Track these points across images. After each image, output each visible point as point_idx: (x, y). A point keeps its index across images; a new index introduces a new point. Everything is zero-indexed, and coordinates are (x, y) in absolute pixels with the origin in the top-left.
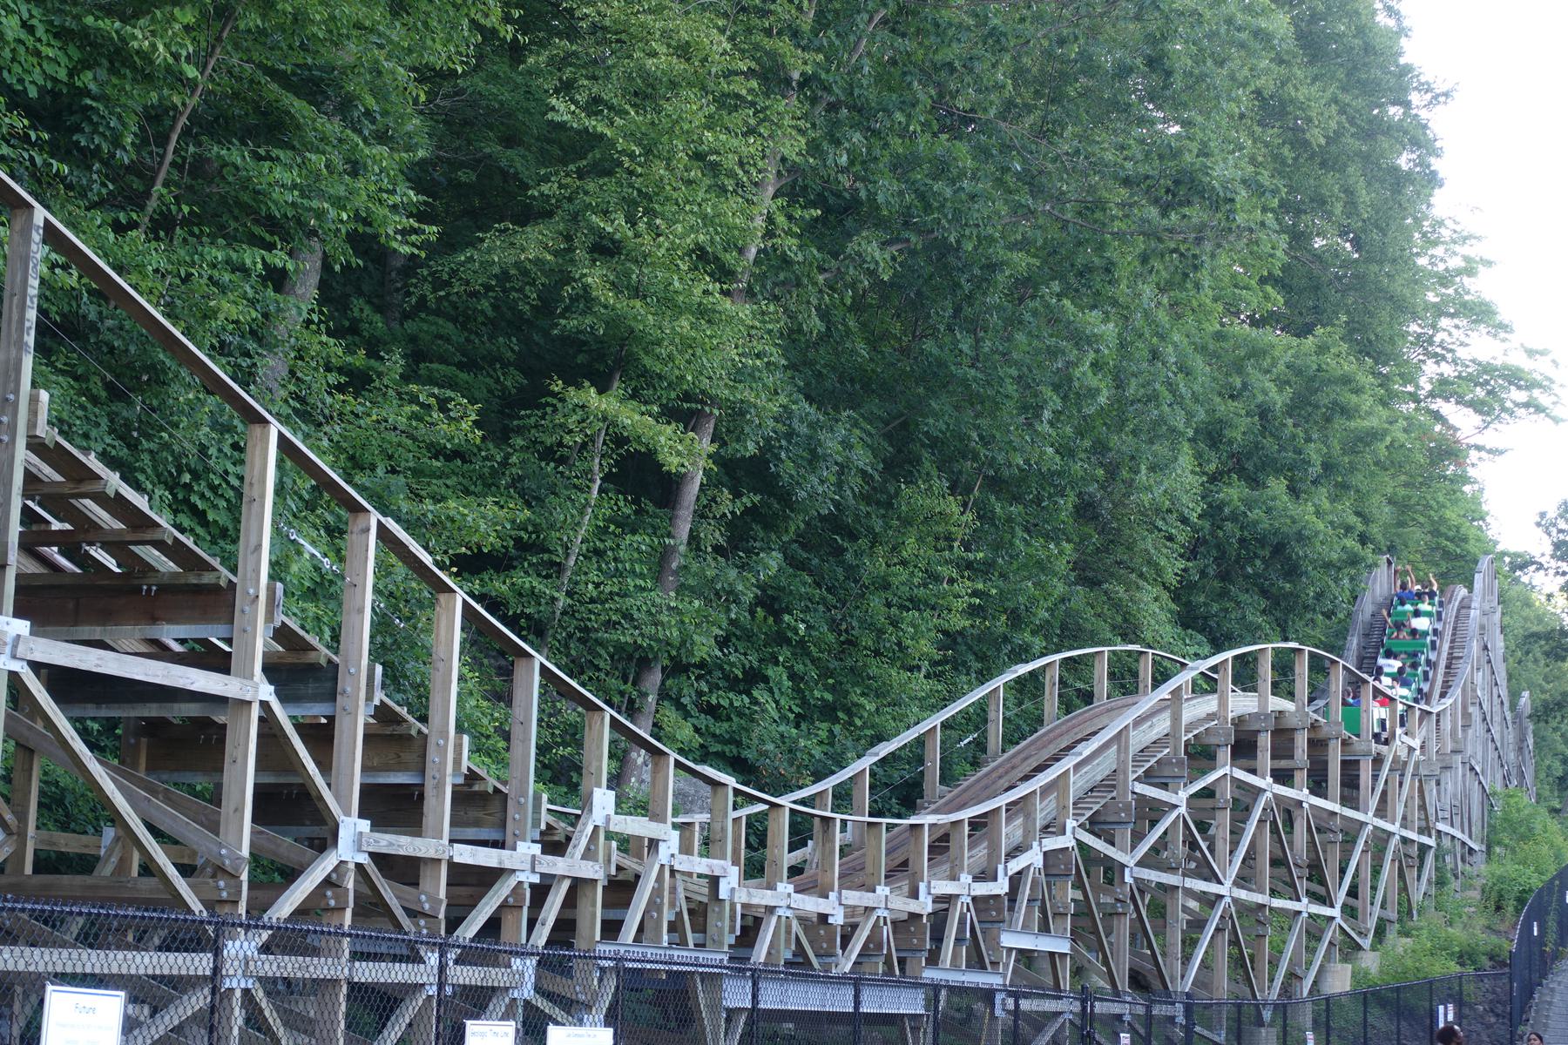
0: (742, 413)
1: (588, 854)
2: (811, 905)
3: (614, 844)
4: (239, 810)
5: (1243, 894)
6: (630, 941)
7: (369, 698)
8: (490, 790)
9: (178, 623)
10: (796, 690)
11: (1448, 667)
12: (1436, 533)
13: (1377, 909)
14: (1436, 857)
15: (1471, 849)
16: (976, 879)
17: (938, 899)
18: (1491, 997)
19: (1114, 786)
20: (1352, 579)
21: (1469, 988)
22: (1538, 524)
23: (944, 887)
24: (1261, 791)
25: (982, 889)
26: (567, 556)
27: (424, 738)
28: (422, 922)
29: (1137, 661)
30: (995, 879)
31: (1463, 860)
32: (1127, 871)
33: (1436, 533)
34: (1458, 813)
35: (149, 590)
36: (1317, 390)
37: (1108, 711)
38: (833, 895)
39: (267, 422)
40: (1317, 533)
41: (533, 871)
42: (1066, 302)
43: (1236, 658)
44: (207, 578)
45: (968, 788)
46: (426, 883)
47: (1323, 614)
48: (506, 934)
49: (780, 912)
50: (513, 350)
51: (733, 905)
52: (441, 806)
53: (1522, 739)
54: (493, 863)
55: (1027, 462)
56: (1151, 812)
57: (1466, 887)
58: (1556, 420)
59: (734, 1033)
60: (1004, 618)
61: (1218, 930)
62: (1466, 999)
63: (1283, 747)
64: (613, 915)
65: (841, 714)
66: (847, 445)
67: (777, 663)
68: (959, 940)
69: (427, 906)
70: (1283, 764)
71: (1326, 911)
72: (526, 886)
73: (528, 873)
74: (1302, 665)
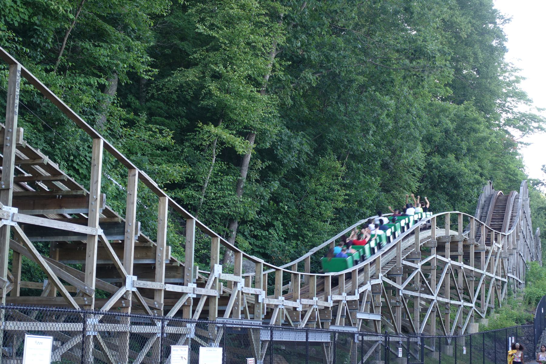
1: (213, 287)
2: (291, 304)
3: (222, 284)
4: (91, 273)
5: (441, 299)
7: (136, 234)
8: (179, 265)
9: (69, 208)
10: (284, 229)
11: (511, 219)
12: (506, 173)
14: (508, 286)
15: (520, 283)
17: (335, 302)
18: (527, 334)
19: (395, 262)
20: (477, 189)
21: (520, 331)
22: (542, 169)
23: (337, 298)
24: (447, 263)
25: (350, 298)
26: (204, 183)
28: (155, 312)
30: (354, 294)
31: (517, 287)
32: (400, 291)
33: (506, 173)
34: (515, 270)
38: (298, 301)
40: (465, 173)
41: (194, 293)
42: (377, 93)
44: (79, 193)
46: (156, 298)
49: (280, 307)
52: (161, 271)
53: (537, 244)
54: (180, 291)
55: (364, 149)
56: (408, 271)
57: (518, 296)
60: (356, 203)
61: (432, 311)
62: (518, 335)
63: (454, 248)
64: (222, 308)
65: (300, 238)
66: (301, 144)
67: (278, 220)
68: (342, 316)
69: (157, 306)
70: (454, 253)
71: (469, 305)
72: (191, 299)
73: (192, 294)
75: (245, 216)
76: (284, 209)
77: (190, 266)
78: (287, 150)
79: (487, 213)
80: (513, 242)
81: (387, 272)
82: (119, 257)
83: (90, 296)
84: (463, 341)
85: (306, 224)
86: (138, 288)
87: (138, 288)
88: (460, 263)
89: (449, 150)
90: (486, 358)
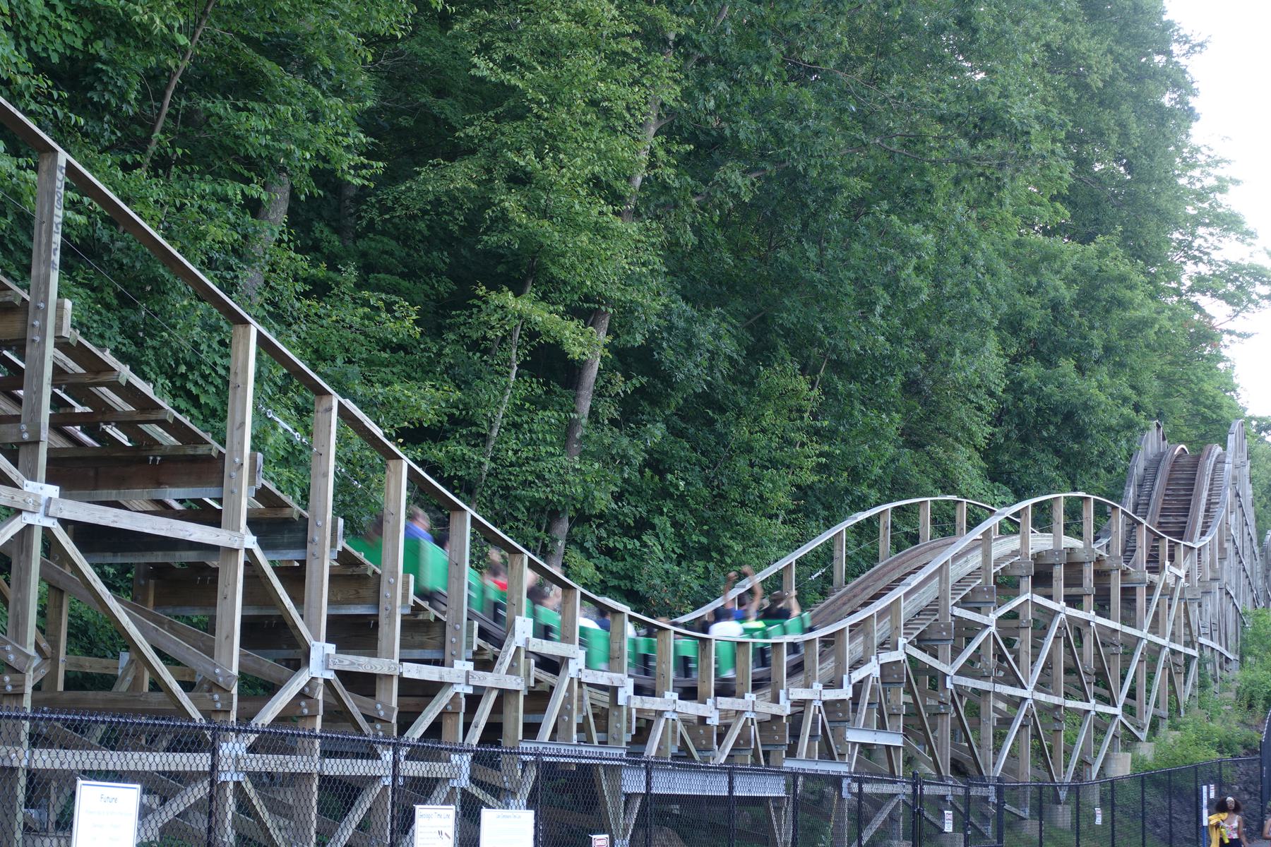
1: (512, 670)
4: (230, 637)
5: (1042, 697)
7: (333, 545)
8: (432, 619)
11: (1207, 511)
12: (1196, 402)
13: (1151, 708)
14: (1199, 666)
15: (1227, 660)
17: (795, 704)
18: (1245, 778)
19: (937, 610)
20: (1128, 441)
21: (1227, 771)
23: (800, 694)
24: (1056, 613)
25: (831, 695)
26: (491, 428)
27: (378, 577)
28: (378, 726)
30: (841, 687)
31: (1221, 668)
32: (948, 679)
33: (1196, 402)
34: (1216, 629)
35: (155, 460)
36: (1098, 287)
38: (710, 701)
39: (248, 323)
40: (1100, 404)
41: (467, 684)
42: (894, 217)
43: (1034, 505)
46: (381, 694)
47: (1105, 469)
49: (668, 715)
50: (445, 263)
51: (629, 710)
54: (435, 678)
55: (863, 348)
56: (967, 631)
57: (1223, 690)
60: (845, 474)
61: (1022, 726)
62: (1224, 780)
64: (533, 719)
65: (714, 554)
67: (662, 514)
68: (813, 736)
69: (382, 713)
70: (1074, 591)
73: (463, 686)
78: (683, 351)
79: (1150, 496)
83: (227, 691)
84: (1094, 796)
89: (1061, 349)
90: (1148, 834)
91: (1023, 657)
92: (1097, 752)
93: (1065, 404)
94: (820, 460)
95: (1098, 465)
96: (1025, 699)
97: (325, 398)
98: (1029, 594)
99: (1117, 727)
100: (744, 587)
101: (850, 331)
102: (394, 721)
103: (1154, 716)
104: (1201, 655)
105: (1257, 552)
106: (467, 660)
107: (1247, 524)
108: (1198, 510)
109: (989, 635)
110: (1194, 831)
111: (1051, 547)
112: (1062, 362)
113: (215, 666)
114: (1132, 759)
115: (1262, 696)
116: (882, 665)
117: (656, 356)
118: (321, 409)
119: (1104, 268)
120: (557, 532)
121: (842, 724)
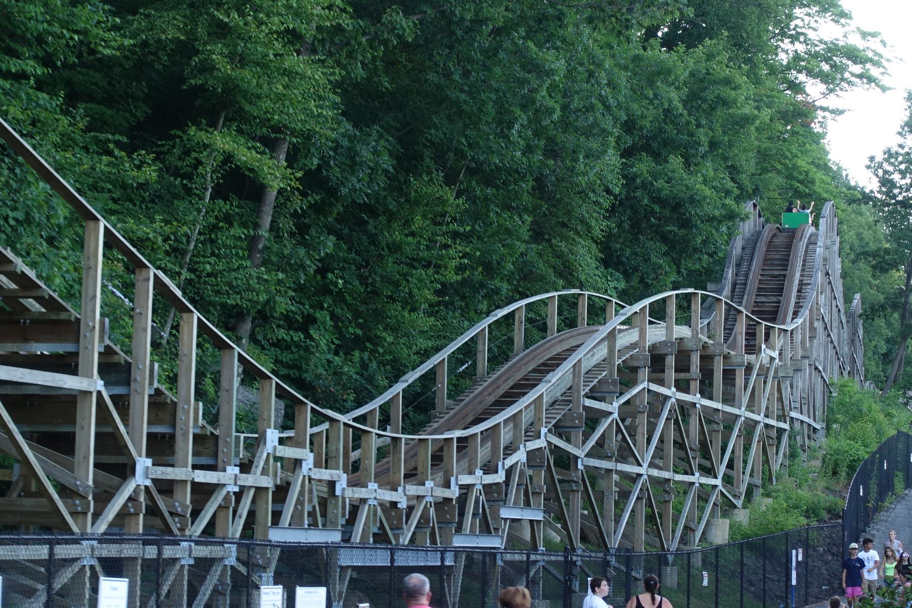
0: (309, 138)
1: (264, 472)
2: (388, 496)
3: (279, 464)
4: (86, 457)
5: (655, 473)
6: (287, 525)
7: (151, 384)
8: (209, 434)
9: (42, 342)
10: (336, 327)
11: (799, 291)
12: (790, 177)
13: (747, 478)
14: (790, 437)
15: (815, 430)
16: (486, 472)
17: (462, 487)
18: (828, 541)
19: (570, 401)
20: (729, 228)
21: (813, 535)
22: (868, 167)
23: (466, 480)
24: (666, 398)
25: (489, 479)
26: (188, 242)
27: (175, 404)
28: (177, 520)
29: (577, 299)
30: (496, 472)
31: (809, 437)
32: (579, 461)
33: (790, 177)
34: (806, 404)
35: (25, 322)
36: (705, 88)
37: (560, 341)
38: (400, 489)
39: (98, 220)
40: (705, 198)
41: (235, 484)
42: (530, 44)
43: (651, 304)
44: (63, 316)
45: (469, 403)
46: (177, 495)
47: (707, 254)
48: (258, 535)
49: (370, 502)
50: (143, 92)
51: (344, 499)
52: (186, 447)
53: (854, 333)
54: (214, 481)
55: (501, 161)
56: (593, 419)
57: (812, 457)
58: (884, 89)
59: (344, 580)
60: (480, 269)
61: (638, 498)
62: (811, 542)
63: (683, 366)
64: (278, 508)
65: (368, 345)
66: (375, 153)
67: (322, 308)
68: (475, 515)
69: (179, 510)
70: (683, 375)
71: (712, 481)
72: (231, 494)
73: (232, 486)
74: (696, 303)
75: (267, 308)
76: (336, 284)
77: (230, 436)
78: (347, 168)
79: (747, 275)
80: (803, 342)
81: (554, 422)
82: (124, 425)
83: (85, 498)
84: (697, 561)
85: (379, 315)
86: (154, 481)
87: (154, 481)
88: (694, 398)
89: (669, 145)
90: (745, 592)
91: (639, 437)
92: (700, 519)
93: (673, 198)
94: (462, 261)
95: (701, 252)
96: (642, 475)
97: (144, 271)
98: (646, 383)
99: (717, 496)
100: (407, 381)
101: (491, 147)
102: (188, 516)
103: (749, 484)
104: (791, 428)
105: (844, 321)
106: (235, 466)
107: (835, 298)
108: (791, 291)
109: (613, 421)
110: (784, 589)
111: (664, 339)
112: (672, 158)
113: (76, 479)
114: (730, 525)
115: (845, 464)
116: (528, 452)
117: (325, 173)
118: (140, 278)
119: (711, 71)
120: (242, 331)
121: (497, 503)
